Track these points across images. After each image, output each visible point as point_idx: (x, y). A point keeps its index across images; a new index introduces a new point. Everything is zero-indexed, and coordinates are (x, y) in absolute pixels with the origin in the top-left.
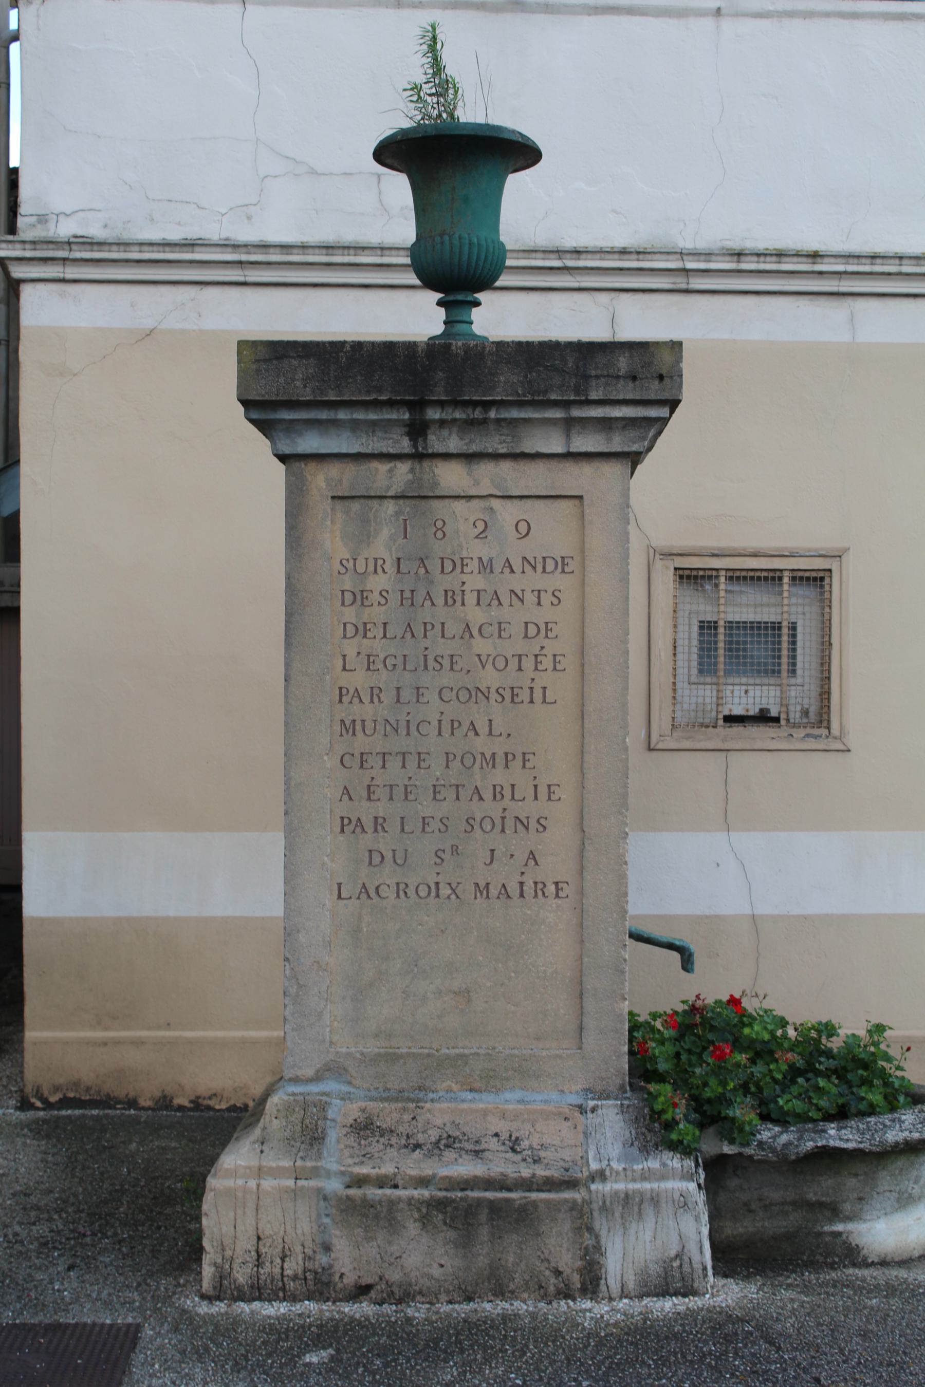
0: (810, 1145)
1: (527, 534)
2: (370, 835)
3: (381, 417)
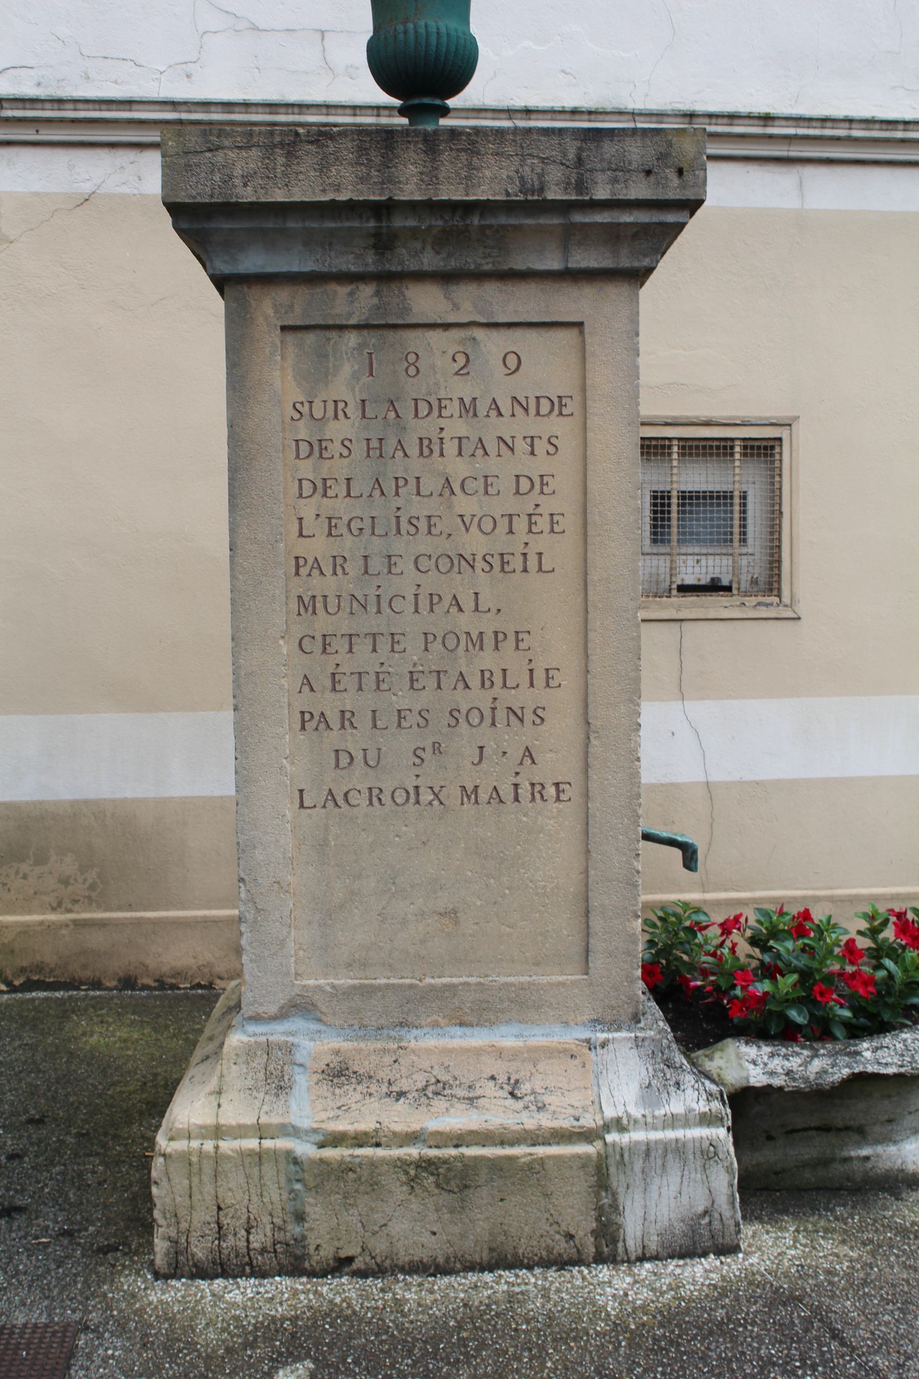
0: (846, 1072)
1: (517, 369)
2: (335, 734)
3: (339, 225)
